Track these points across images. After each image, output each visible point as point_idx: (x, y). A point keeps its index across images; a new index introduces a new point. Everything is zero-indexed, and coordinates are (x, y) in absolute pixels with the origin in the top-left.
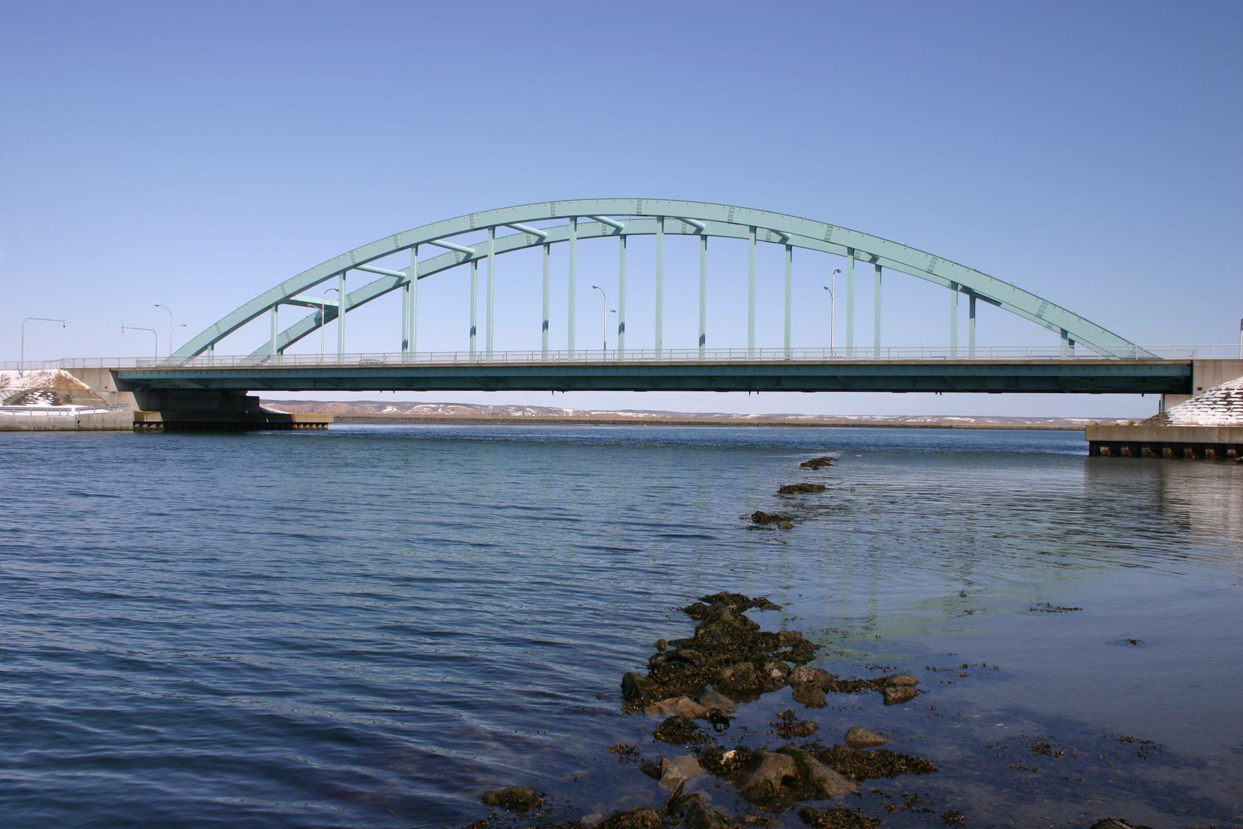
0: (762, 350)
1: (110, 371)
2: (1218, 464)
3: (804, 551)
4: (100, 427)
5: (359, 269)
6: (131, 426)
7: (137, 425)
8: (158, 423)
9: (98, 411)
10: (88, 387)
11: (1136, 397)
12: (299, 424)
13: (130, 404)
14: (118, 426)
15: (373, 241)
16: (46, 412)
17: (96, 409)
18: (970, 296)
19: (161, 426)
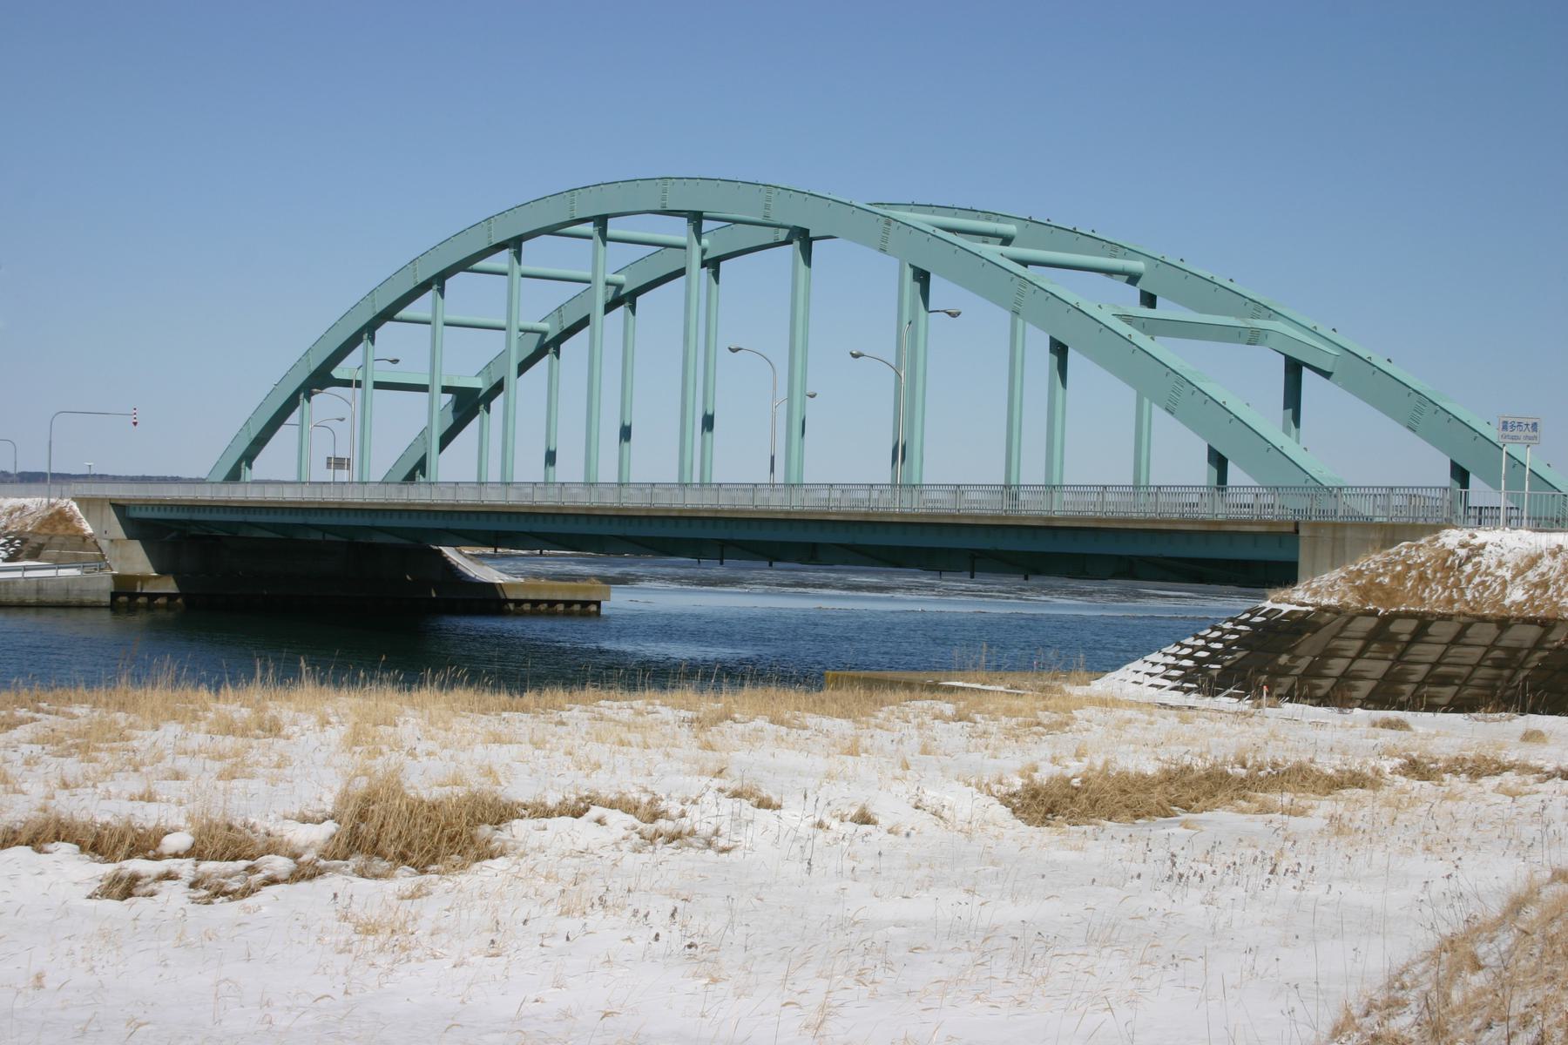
0: (1485, 513)
1: (113, 505)
2: (337, 684)
3: (1162, 806)
4: (32, 599)
5: (401, 320)
6: (107, 599)
7: (123, 599)
8: (170, 596)
9: (63, 572)
10: (88, 529)
11: (1074, 552)
12: (519, 602)
13: (136, 561)
14: (73, 598)
15: (580, 291)
16: (55, 571)
17: (59, 568)
18: (1138, 391)
19: (179, 601)
